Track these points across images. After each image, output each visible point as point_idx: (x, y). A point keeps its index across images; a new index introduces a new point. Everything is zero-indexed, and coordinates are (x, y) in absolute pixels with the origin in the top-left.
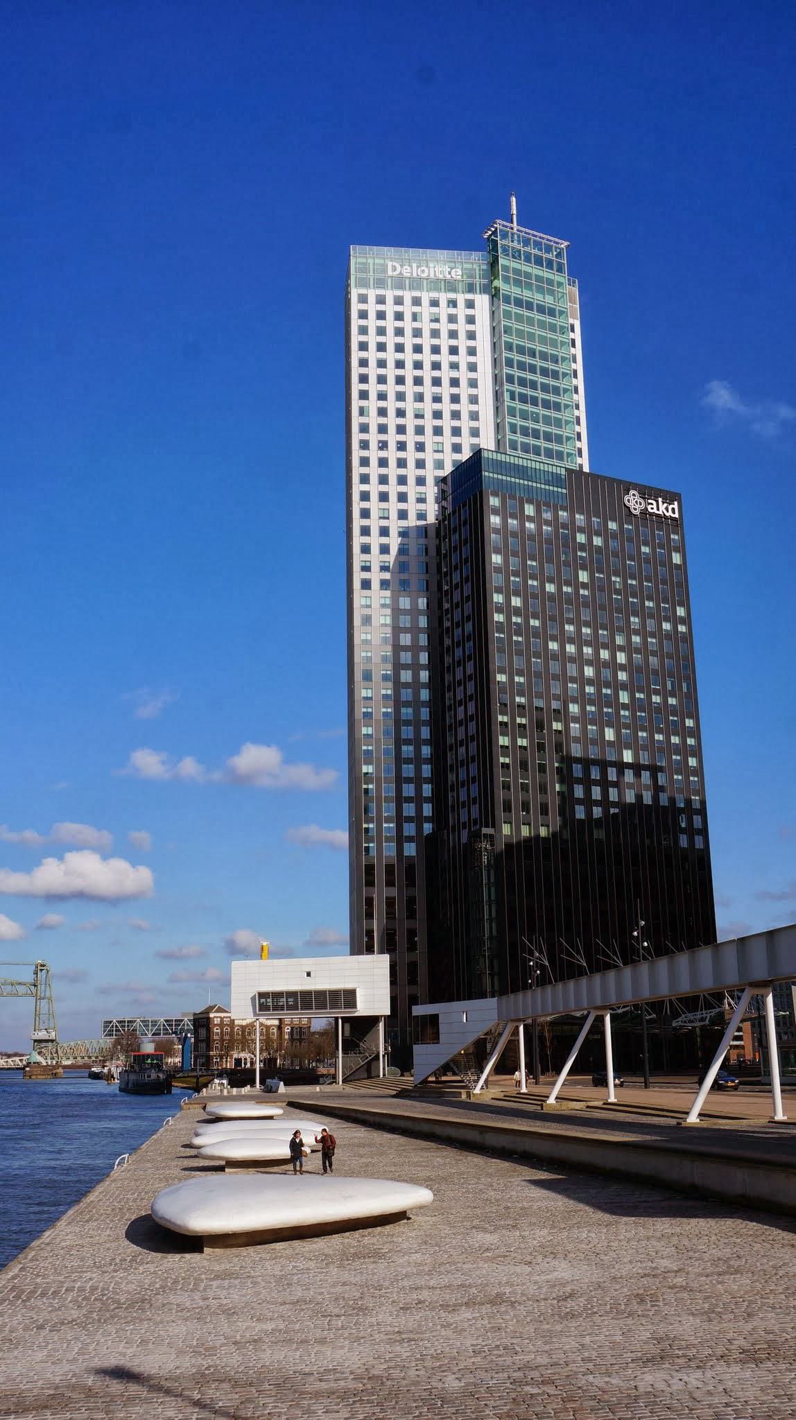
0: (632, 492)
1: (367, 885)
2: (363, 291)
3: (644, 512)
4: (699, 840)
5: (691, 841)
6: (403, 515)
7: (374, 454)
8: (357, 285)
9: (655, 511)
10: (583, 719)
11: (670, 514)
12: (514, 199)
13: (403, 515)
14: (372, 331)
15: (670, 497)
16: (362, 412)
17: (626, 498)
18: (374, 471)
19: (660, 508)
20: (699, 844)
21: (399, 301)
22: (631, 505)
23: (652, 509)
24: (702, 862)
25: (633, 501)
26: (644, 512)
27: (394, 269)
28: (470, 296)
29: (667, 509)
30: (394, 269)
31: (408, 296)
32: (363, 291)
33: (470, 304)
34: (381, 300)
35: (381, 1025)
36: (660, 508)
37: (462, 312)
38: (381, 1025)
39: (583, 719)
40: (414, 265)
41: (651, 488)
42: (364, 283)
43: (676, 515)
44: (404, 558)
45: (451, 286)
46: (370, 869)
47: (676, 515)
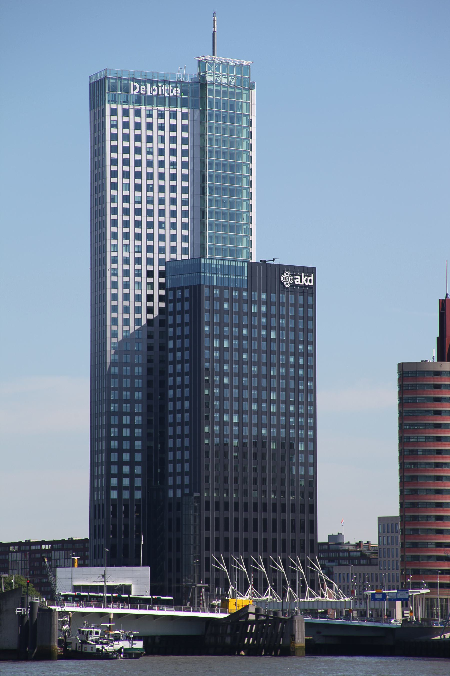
0: (286, 273)
2: (114, 106)
3: (293, 285)
4: (311, 470)
5: (307, 471)
8: (110, 102)
9: (299, 283)
10: (278, 402)
11: (308, 283)
16: (113, 200)
20: (311, 472)
24: (312, 483)
25: (287, 279)
26: (293, 285)
27: (135, 88)
30: (135, 88)
31: (144, 109)
32: (114, 106)
35: (127, 596)
38: (127, 596)
39: (278, 402)
40: (149, 85)
43: (312, 284)
44: (163, 317)
45: (173, 101)
47: (312, 284)
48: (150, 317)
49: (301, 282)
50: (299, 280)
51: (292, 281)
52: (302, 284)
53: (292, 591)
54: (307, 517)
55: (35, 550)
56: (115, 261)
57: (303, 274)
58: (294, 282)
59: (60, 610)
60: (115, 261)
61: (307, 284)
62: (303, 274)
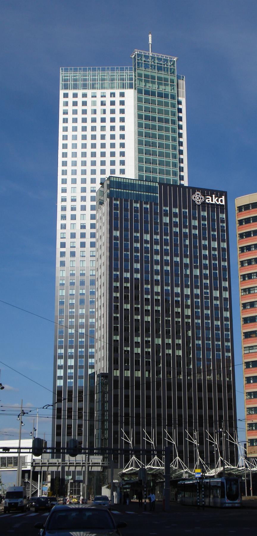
1: (57, 418)
3: (204, 203)
6: (103, 172)
7: (70, 117)
9: (210, 202)
12: (150, 36)
13: (103, 172)
14: (70, 112)
15: (219, 194)
17: (193, 196)
18: (70, 108)
19: (213, 200)
21: (85, 95)
22: (196, 200)
23: (209, 200)
26: (204, 203)
28: (122, 91)
29: (218, 200)
33: (122, 95)
34: (75, 95)
36: (213, 200)
37: (117, 99)
41: (208, 190)
42: (66, 87)
43: (223, 203)
46: (60, 393)
47: (223, 203)
48: (103, 176)
49: (212, 201)
50: (210, 199)
51: (203, 200)
52: (214, 202)
53: (201, 460)
54: (225, 395)
55: (84, 531)
56: (64, 200)
57: (214, 196)
58: (205, 200)
59: (97, 335)
60: (64, 200)
61: (218, 203)
62: (214, 196)
